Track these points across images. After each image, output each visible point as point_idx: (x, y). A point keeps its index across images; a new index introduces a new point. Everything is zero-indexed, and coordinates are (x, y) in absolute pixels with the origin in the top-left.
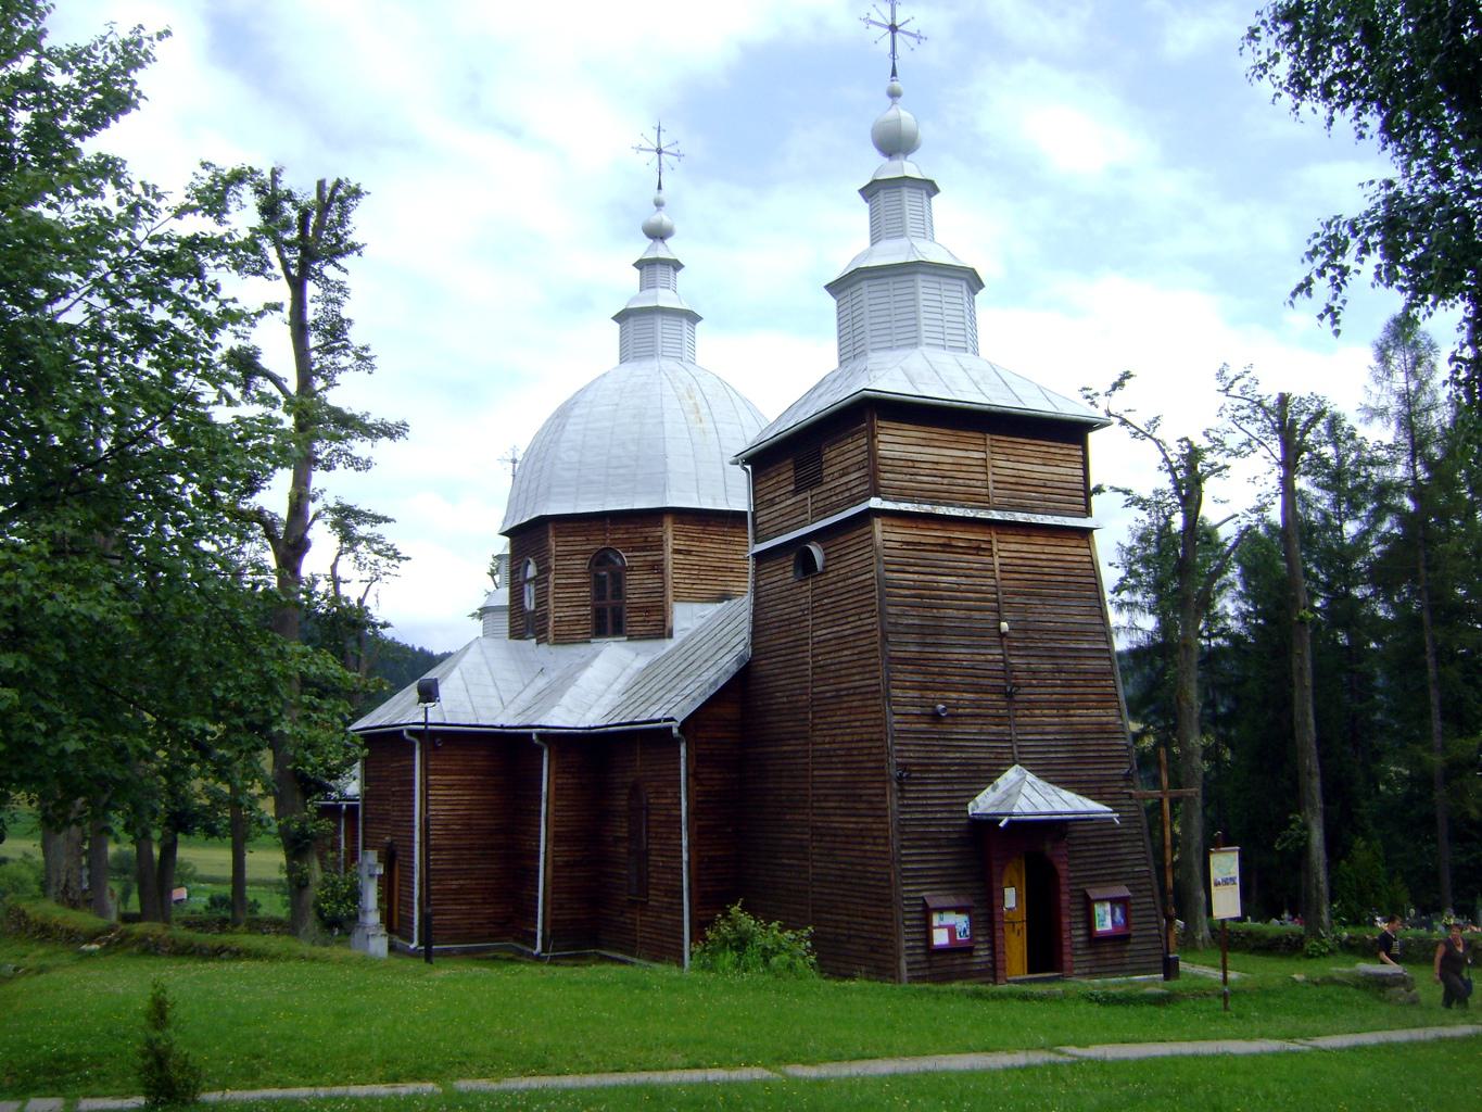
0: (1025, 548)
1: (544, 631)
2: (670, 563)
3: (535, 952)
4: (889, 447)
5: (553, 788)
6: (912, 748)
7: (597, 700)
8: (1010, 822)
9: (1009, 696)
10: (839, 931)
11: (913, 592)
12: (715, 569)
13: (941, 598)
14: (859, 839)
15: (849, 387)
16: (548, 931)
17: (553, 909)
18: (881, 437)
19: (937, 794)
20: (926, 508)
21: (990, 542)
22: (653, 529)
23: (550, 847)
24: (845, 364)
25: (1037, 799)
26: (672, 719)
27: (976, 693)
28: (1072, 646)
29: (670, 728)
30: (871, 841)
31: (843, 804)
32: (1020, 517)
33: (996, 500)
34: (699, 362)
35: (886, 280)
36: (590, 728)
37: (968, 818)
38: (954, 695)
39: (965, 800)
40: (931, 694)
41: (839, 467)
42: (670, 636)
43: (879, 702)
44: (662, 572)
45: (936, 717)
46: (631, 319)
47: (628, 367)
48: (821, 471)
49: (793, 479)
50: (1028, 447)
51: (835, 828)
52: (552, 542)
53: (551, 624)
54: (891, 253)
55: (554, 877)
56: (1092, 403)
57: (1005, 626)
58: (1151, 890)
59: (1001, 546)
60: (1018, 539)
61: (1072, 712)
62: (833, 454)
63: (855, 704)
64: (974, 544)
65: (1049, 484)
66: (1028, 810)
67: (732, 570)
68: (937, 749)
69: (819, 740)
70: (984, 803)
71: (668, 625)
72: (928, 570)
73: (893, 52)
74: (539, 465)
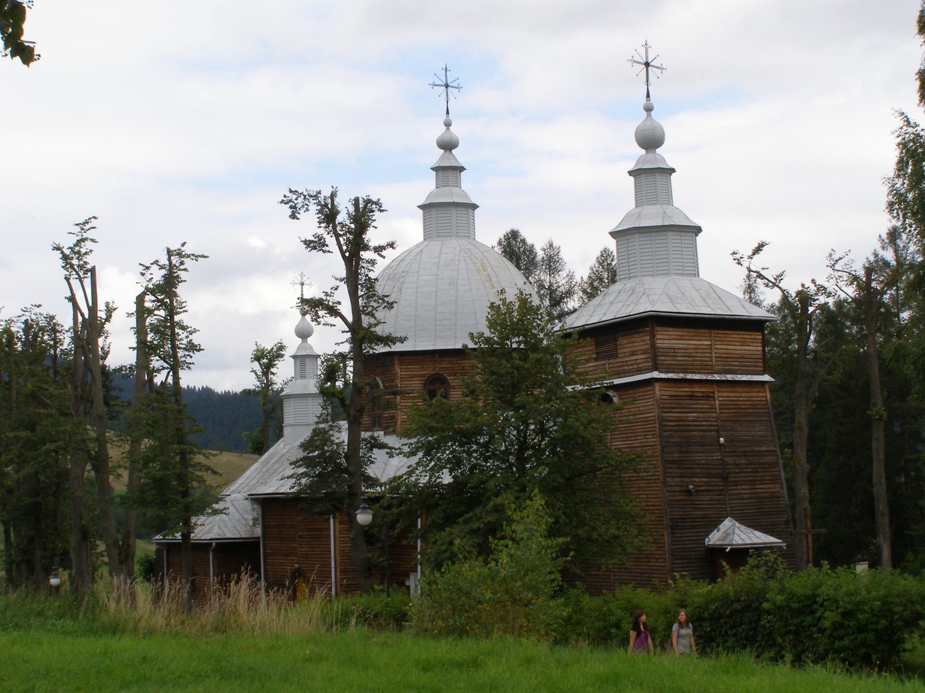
0: (732, 395)
8: (731, 549)
9: (725, 479)
13: (690, 426)
20: (681, 376)
21: (713, 392)
25: (743, 536)
32: (729, 377)
33: (717, 368)
38: (697, 480)
40: (685, 479)
45: (689, 492)
47: (435, 245)
52: (397, 369)
54: (652, 217)
56: (739, 263)
57: (722, 440)
59: (720, 394)
60: (728, 389)
66: (740, 542)
70: (714, 538)
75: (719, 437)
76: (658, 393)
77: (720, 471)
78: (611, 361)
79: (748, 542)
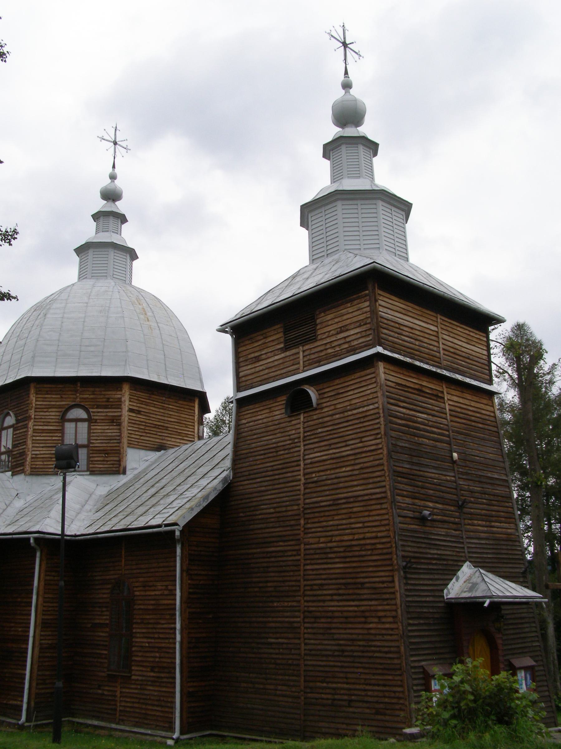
0: (461, 400)
1: (23, 465)
2: (126, 419)
3: (20, 722)
4: (385, 310)
5: (42, 583)
6: (409, 544)
7: (76, 516)
8: (491, 603)
9: (460, 507)
10: (336, 697)
11: (404, 422)
12: (156, 426)
14: (363, 620)
15: (92, 372)
16: (33, 704)
17: (37, 684)
18: (380, 302)
19: (426, 582)
20: (408, 360)
22: (114, 393)
23: (37, 631)
24: (314, 261)
26: (175, 524)
27: (443, 504)
28: (489, 475)
29: (173, 532)
30: (376, 620)
31: (341, 592)
32: (459, 377)
34: (133, 284)
35: (355, 202)
36: (76, 536)
37: (444, 602)
39: (442, 587)
41: (335, 326)
42: (124, 473)
43: (384, 506)
44: (119, 424)
45: (423, 520)
46: (91, 252)
47: (89, 283)
48: (315, 331)
49: (282, 340)
50: (459, 329)
51: (333, 612)
52: (33, 397)
53: (29, 459)
55: (39, 657)
57: (455, 455)
58: (542, 660)
61: (493, 524)
62: (329, 317)
63: (355, 510)
64: (435, 392)
65: (471, 357)
67: (167, 428)
68: (424, 546)
69: (311, 540)
70: (455, 589)
71: (123, 464)
72: (411, 406)
73: (345, 59)
74: (22, 342)
75: (451, 452)
76: (382, 376)
77: (454, 497)
78: (305, 348)
79: (508, 594)
